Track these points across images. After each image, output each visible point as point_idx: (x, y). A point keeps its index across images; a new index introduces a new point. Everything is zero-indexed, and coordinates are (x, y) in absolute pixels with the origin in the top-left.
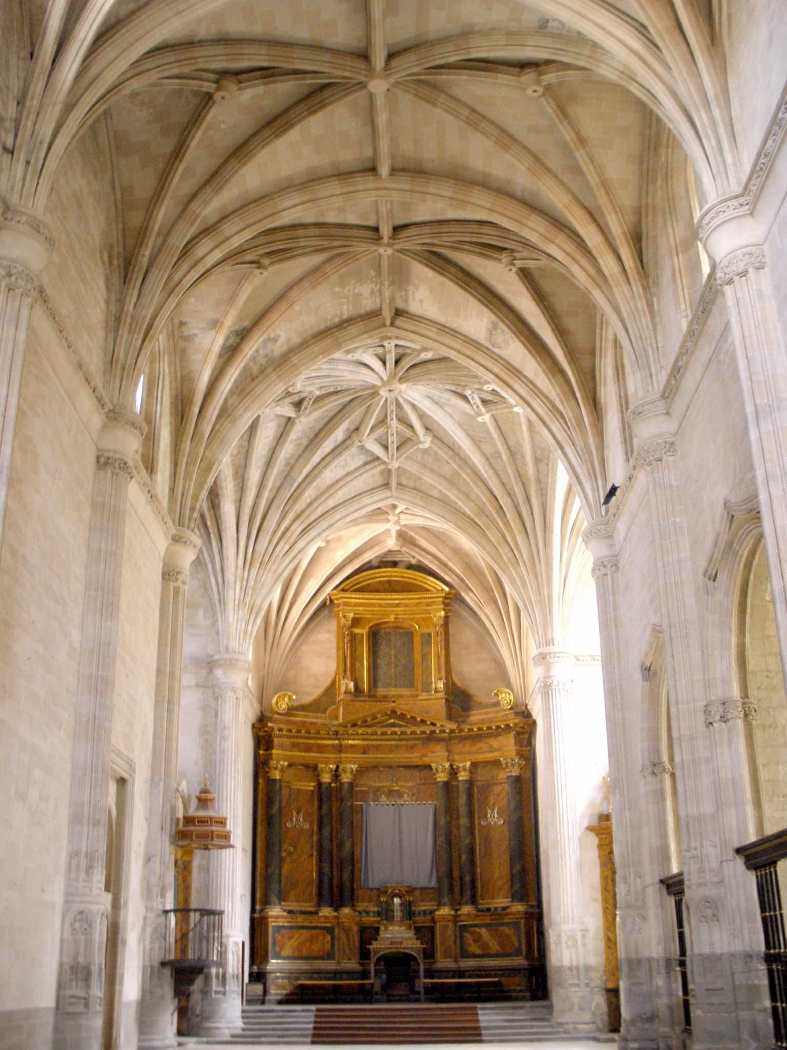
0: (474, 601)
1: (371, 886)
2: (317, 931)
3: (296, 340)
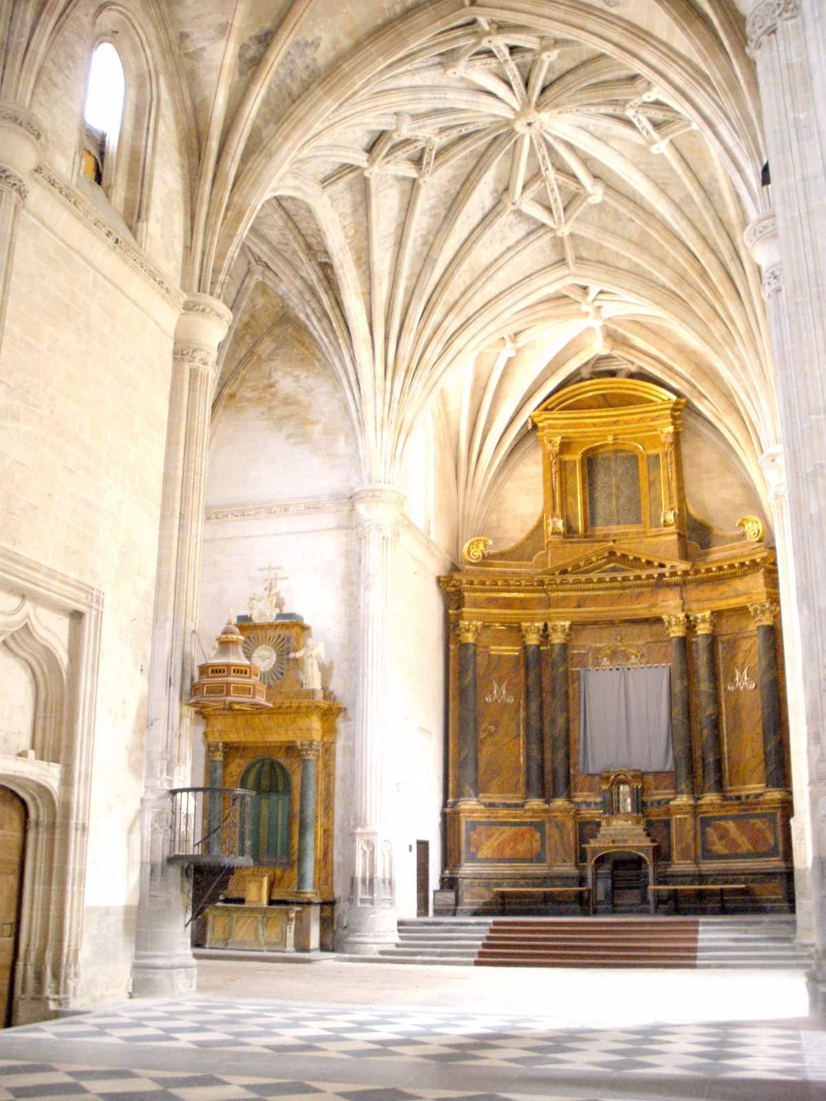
0: (712, 412)
1: (591, 771)
2: (523, 828)
3: (346, 42)
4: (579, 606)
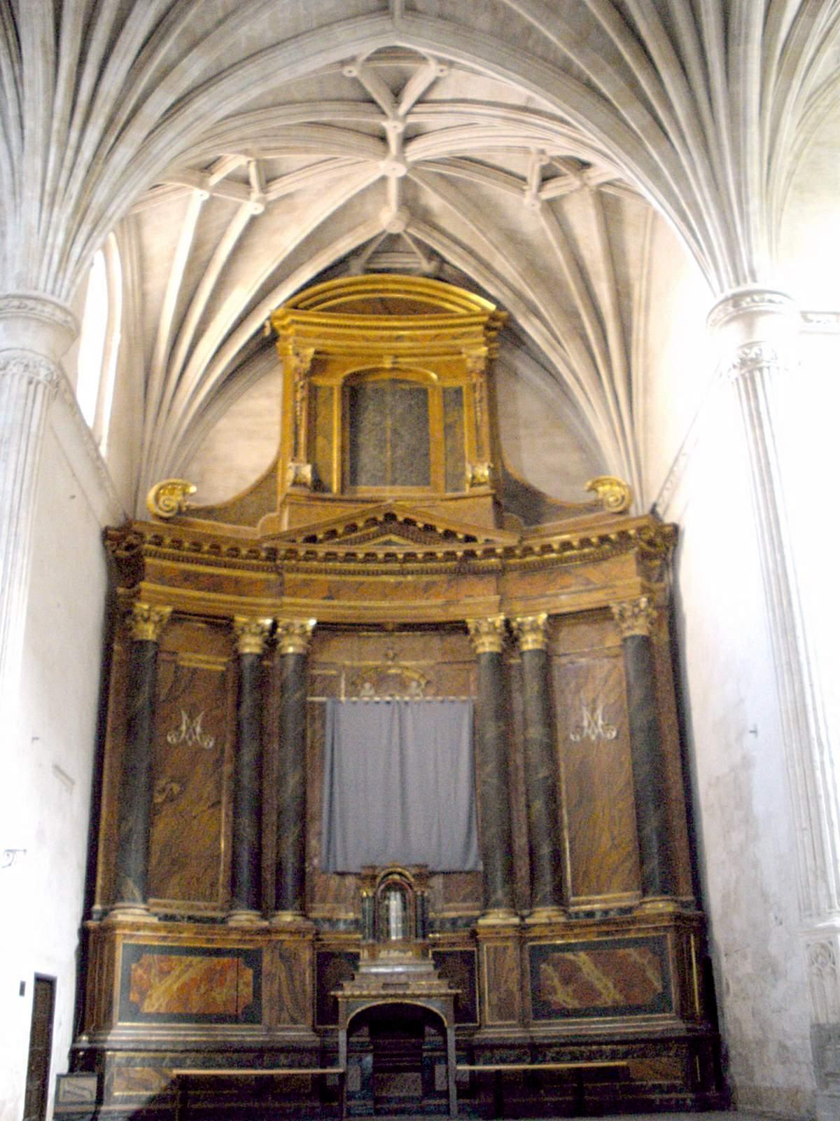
0: (542, 334)
2: (225, 960)
4: (330, 598)
